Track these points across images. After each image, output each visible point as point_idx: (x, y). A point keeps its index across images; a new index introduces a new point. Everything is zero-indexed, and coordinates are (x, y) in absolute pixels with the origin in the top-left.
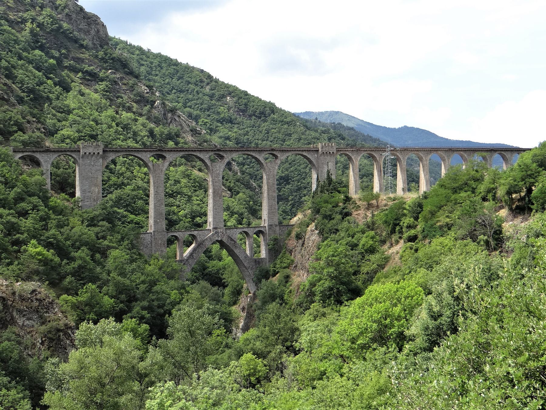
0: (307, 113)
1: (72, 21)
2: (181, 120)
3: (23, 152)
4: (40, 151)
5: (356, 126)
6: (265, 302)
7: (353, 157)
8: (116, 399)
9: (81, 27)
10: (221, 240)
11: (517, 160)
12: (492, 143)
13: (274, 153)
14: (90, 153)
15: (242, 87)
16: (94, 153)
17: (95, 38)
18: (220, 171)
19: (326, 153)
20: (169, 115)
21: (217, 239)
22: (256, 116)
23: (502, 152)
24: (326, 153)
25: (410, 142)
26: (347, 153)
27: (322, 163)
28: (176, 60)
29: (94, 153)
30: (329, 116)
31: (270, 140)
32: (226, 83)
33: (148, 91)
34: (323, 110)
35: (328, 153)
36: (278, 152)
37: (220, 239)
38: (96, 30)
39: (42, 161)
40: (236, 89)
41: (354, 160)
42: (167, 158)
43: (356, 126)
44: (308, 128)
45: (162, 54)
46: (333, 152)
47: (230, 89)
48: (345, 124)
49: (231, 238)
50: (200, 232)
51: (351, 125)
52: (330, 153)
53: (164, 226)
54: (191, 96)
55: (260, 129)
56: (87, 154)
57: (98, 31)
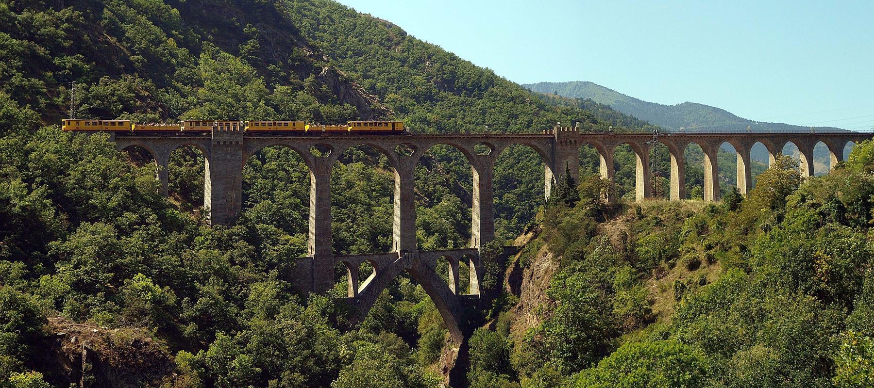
4: (174, 139)
13: (490, 141)
35: (568, 141)
36: (494, 140)
44: (541, 107)
46: (575, 141)
52: (570, 141)
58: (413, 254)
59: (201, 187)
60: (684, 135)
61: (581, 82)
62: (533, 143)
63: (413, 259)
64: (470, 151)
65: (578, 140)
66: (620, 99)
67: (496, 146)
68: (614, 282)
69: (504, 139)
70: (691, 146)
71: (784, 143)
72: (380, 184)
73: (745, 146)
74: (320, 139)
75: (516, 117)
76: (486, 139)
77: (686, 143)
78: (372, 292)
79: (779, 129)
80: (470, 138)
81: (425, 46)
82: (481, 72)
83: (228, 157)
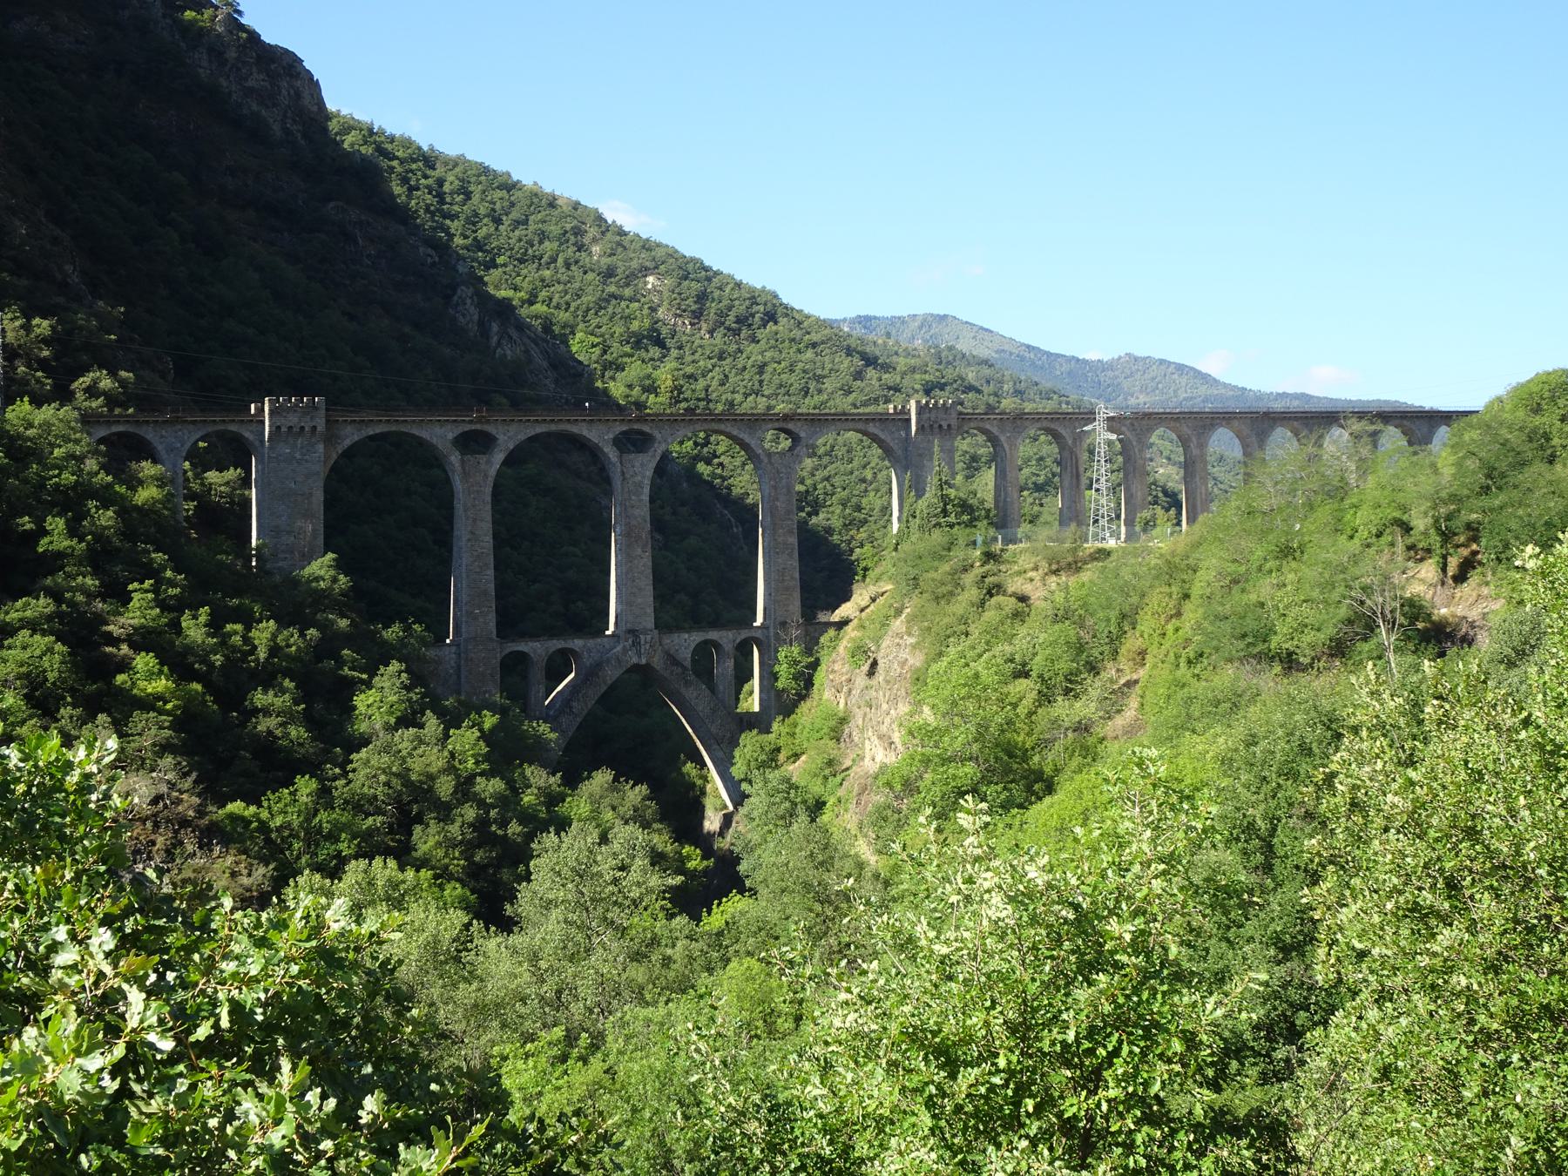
0: (866, 321)
1: (227, 69)
2: (526, 340)
3: (109, 424)
4: (194, 422)
5: (993, 354)
6: (1071, 904)
7: (1003, 438)
8: (125, 987)
9: (250, 83)
10: (648, 665)
11: (1442, 445)
12: (1364, 398)
13: (790, 426)
14: (290, 428)
15: (688, 249)
16: (302, 428)
17: (289, 114)
18: (644, 477)
19: (931, 426)
20: (494, 324)
21: (635, 660)
22: (729, 329)
23: (1405, 422)
24: (931, 426)
25: (1142, 398)
26: (988, 427)
27: (920, 455)
28: (508, 174)
29: (302, 428)
30: (920, 328)
31: (766, 393)
32: (644, 236)
33: (437, 259)
34: (903, 312)
35: (936, 426)
36: (799, 424)
37: (644, 661)
38: (292, 92)
39: (160, 448)
40: (673, 254)
41: (1005, 445)
42: (500, 442)
43: (993, 354)
44: (870, 361)
45: (469, 157)
46: (949, 426)
47: (659, 253)
48: (964, 346)
49: (674, 659)
50: (591, 643)
51: (983, 352)
52: (940, 426)
53: (492, 625)
54: (547, 273)
55: (740, 363)
56: (284, 429)
57: (298, 95)
58: (649, 637)
59: (263, 422)
60: (1148, 416)
61: (932, 315)
62: (872, 428)
63: (648, 646)
64: (753, 443)
65: (954, 423)
66: (1006, 347)
67: (802, 435)
68: (1197, 794)
69: (819, 421)
70: (1160, 431)
71: (1272, 428)
72: (1076, 907)
73: (1258, 435)
74: (471, 422)
75: (819, 379)
76: (784, 425)
77: (1150, 430)
78: (571, 708)
79: (1296, 403)
80: (755, 421)
81: (647, 246)
82: (754, 297)
83: (298, 456)
